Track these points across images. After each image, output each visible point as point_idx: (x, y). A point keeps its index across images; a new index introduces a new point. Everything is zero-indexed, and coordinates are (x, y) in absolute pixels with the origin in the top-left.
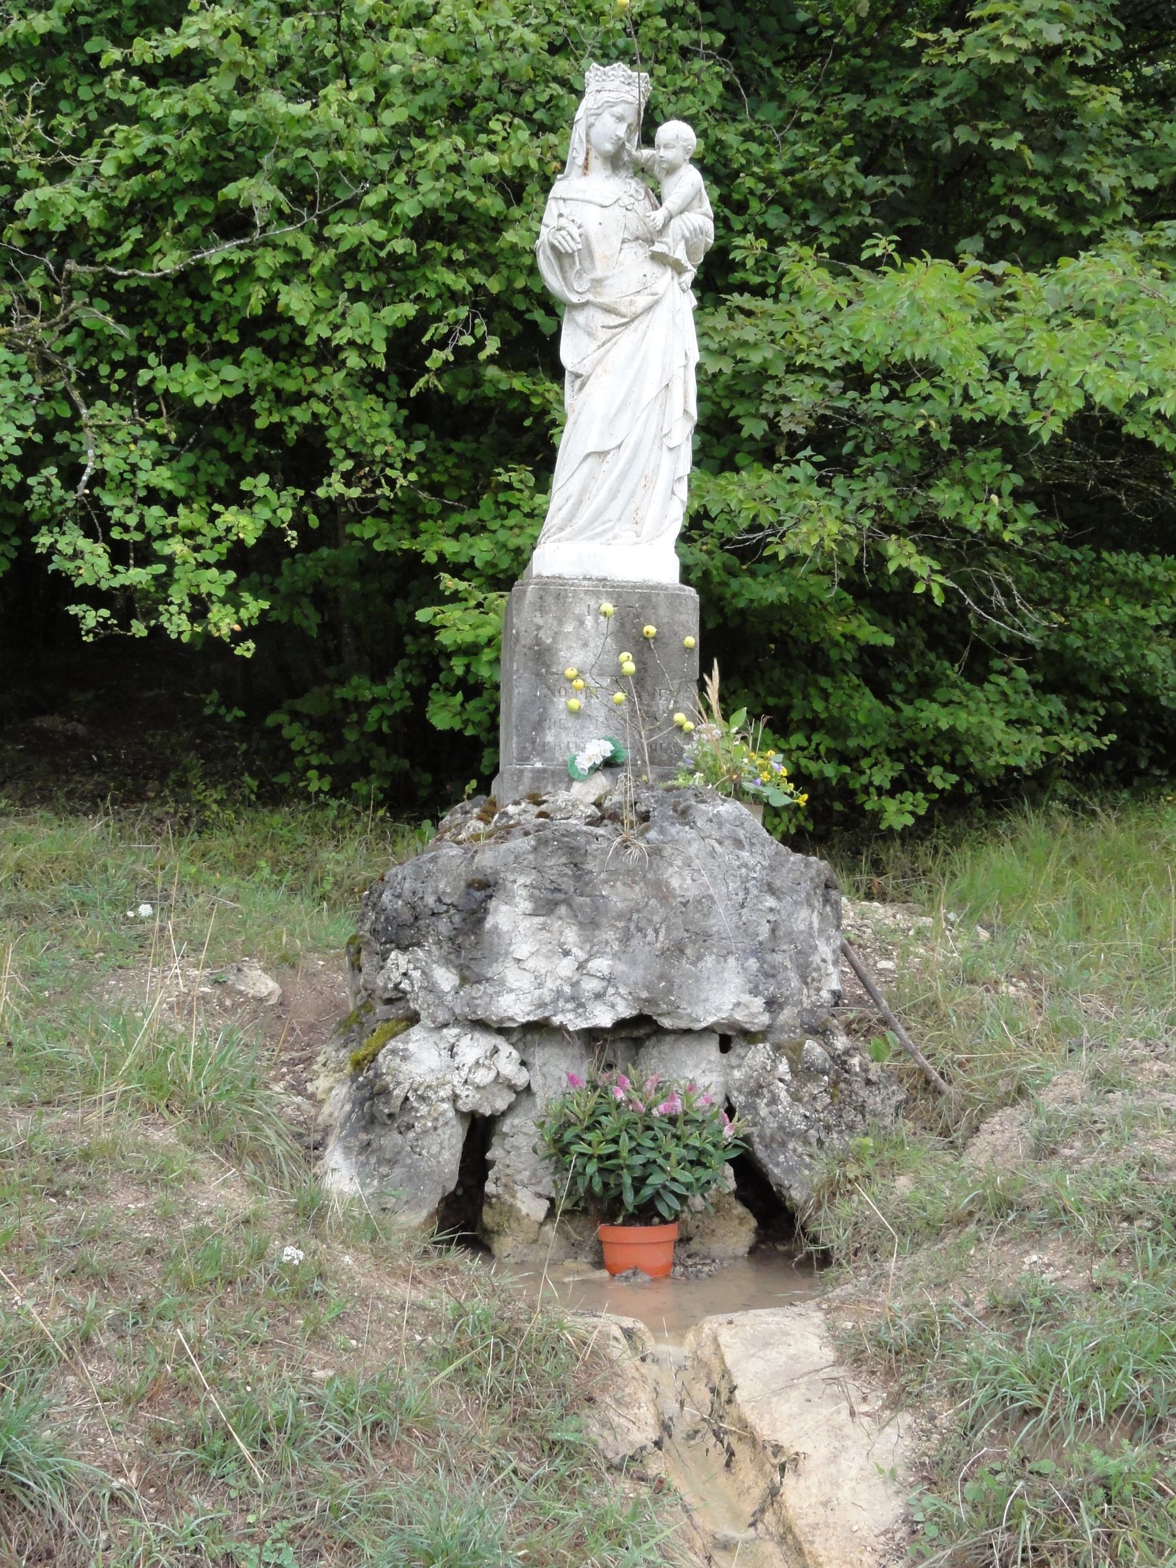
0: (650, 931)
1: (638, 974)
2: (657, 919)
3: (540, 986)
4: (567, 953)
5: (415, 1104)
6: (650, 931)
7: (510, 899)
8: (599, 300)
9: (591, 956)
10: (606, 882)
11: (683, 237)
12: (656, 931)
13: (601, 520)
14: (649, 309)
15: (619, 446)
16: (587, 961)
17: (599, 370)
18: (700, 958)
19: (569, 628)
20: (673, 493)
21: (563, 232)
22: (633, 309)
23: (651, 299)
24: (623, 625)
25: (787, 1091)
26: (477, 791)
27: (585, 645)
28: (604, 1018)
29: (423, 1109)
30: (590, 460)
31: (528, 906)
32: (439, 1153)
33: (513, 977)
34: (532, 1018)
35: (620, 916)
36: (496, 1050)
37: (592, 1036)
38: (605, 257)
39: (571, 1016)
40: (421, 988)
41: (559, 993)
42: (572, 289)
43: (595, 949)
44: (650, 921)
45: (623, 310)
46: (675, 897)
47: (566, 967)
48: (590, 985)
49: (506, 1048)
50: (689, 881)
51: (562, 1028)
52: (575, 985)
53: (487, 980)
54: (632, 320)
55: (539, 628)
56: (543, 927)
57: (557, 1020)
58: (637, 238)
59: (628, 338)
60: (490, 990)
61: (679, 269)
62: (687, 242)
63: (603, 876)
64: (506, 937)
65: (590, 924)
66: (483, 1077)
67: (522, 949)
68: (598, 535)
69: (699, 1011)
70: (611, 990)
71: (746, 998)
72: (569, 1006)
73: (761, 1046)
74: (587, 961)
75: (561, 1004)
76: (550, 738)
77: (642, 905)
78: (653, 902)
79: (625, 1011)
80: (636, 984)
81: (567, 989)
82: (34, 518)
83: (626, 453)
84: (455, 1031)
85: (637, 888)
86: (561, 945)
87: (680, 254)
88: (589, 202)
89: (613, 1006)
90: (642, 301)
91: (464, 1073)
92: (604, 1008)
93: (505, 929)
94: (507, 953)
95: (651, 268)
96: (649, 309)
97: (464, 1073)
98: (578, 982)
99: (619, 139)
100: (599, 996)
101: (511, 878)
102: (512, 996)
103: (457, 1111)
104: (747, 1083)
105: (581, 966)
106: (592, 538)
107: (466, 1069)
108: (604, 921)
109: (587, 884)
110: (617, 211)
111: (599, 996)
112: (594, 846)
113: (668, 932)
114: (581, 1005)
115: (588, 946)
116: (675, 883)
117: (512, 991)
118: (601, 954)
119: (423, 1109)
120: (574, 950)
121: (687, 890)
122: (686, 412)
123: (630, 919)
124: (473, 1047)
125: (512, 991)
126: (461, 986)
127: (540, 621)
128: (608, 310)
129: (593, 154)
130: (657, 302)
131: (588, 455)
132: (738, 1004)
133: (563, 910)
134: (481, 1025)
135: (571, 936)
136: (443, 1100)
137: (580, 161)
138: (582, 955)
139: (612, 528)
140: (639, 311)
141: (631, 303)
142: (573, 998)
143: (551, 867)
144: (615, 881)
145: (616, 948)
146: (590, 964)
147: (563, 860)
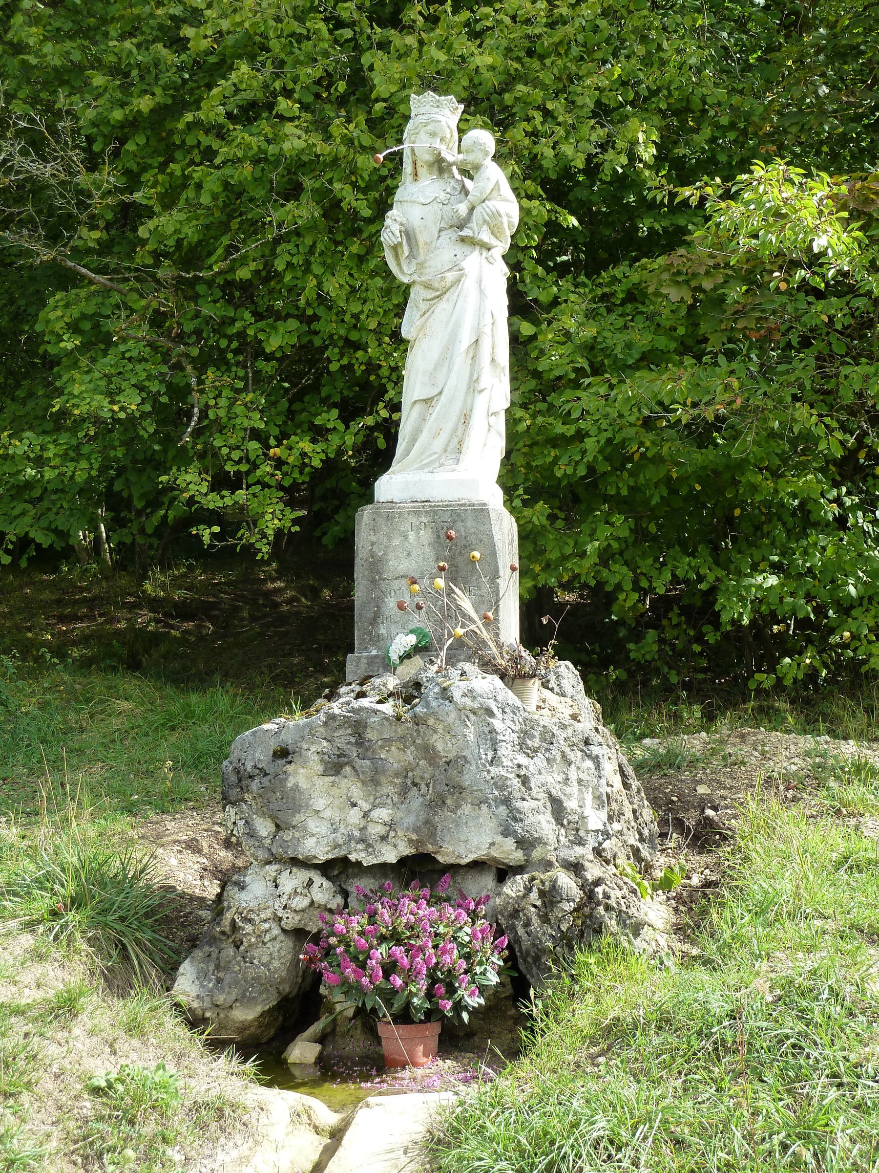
0: (423, 786)
1: (410, 820)
2: (427, 776)
3: (335, 831)
4: (354, 805)
5: (241, 924)
6: (423, 786)
7: (305, 764)
9: (374, 807)
10: (382, 747)
12: (428, 785)
15: (440, 393)
16: (370, 811)
18: (458, 807)
19: (396, 542)
22: (443, 284)
24: (438, 537)
25: (538, 915)
27: (409, 555)
28: (391, 856)
29: (249, 928)
31: (320, 768)
32: (270, 962)
33: (313, 825)
34: (330, 856)
35: (397, 775)
36: (310, 882)
37: (383, 869)
38: (426, 244)
39: (363, 854)
40: (244, 834)
41: (350, 838)
42: (403, 272)
43: (377, 801)
44: (422, 778)
45: (436, 285)
46: (441, 758)
47: (354, 816)
48: (376, 830)
49: (319, 880)
50: (450, 745)
51: (359, 864)
52: (363, 829)
53: (294, 827)
55: (373, 544)
56: (333, 784)
57: (353, 857)
58: (452, 227)
59: (443, 306)
60: (297, 835)
63: (380, 743)
64: (306, 792)
65: (373, 781)
66: (300, 903)
67: (320, 803)
69: (462, 850)
70: (392, 834)
71: (499, 839)
72: (360, 846)
73: (518, 877)
74: (370, 811)
75: (353, 844)
76: (382, 631)
77: (414, 765)
78: (422, 762)
79: (406, 850)
80: (408, 829)
81: (357, 833)
82: (273, 463)
84: (275, 867)
85: (408, 752)
86: (349, 799)
88: (414, 202)
89: (395, 846)
90: (450, 276)
91: (284, 900)
92: (389, 847)
93: (304, 786)
94: (307, 806)
95: (459, 249)
96: (458, 281)
97: (284, 900)
98: (365, 828)
100: (384, 838)
101: (305, 746)
102: (314, 839)
103: (284, 931)
104: (505, 908)
105: (366, 815)
106: (422, 468)
107: (286, 897)
108: (383, 779)
109: (367, 749)
110: (436, 206)
111: (384, 838)
112: (373, 720)
113: (434, 787)
114: (369, 845)
115: (372, 799)
116: (439, 746)
117: (313, 835)
118: (383, 805)
119: (249, 928)
120: (360, 802)
121: (449, 751)
123: (406, 777)
124: (290, 881)
125: (313, 835)
126: (277, 831)
127: (374, 539)
129: (419, 164)
131: (415, 402)
132: (493, 844)
133: (348, 770)
134: (296, 862)
135: (357, 792)
136: (265, 921)
138: (366, 806)
139: (439, 458)
141: (443, 278)
142: (362, 840)
143: (340, 737)
144: (390, 746)
145: (395, 799)
146: (372, 813)
147: (349, 731)
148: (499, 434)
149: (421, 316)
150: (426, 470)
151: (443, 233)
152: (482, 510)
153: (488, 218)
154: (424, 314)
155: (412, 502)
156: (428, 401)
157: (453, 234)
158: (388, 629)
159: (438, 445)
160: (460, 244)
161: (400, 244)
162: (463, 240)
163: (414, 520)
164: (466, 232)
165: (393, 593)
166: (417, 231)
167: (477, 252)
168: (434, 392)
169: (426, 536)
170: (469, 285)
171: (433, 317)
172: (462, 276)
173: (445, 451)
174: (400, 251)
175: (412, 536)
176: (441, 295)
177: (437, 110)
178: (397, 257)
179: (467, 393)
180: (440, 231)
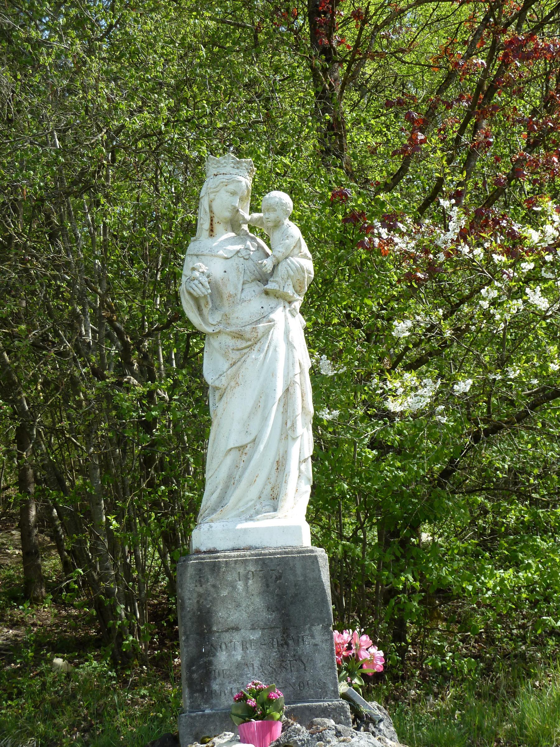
24: (268, 586)
30: (233, 453)
38: (230, 296)
45: (248, 336)
88: (216, 256)
95: (267, 302)
129: (215, 220)
131: (230, 450)
137: (207, 226)
148: (309, 480)
149: (232, 365)
151: (246, 286)
152: (310, 557)
153: (291, 273)
154: (234, 364)
155: (233, 550)
156: (241, 448)
157: (257, 288)
158: (222, 685)
159: (254, 492)
160: (264, 295)
162: (267, 293)
164: (271, 286)
165: (224, 647)
168: (250, 438)
169: (254, 585)
170: (277, 334)
172: (271, 327)
175: (240, 586)
176: (252, 345)
177: (237, 171)
179: (280, 439)
180: (243, 284)
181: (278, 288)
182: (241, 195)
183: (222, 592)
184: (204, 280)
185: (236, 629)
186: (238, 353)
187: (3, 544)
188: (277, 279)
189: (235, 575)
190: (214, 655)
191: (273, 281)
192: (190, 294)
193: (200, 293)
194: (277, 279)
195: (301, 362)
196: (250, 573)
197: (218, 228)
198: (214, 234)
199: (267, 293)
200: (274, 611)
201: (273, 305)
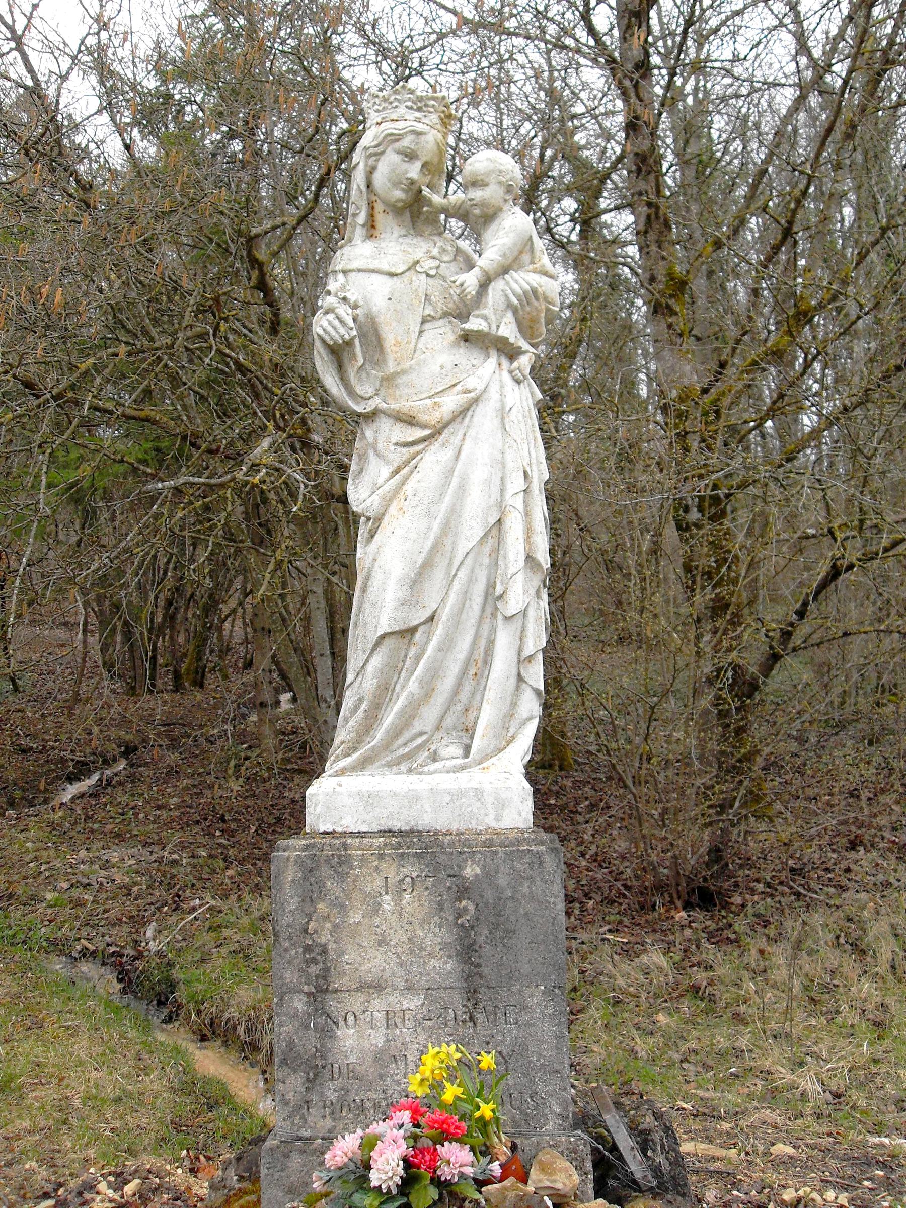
8: (394, 406)
11: (510, 305)
13: (407, 735)
14: (462, 413)
15: (432, 618)
17: (393, 510)
19: (355, 917)
20: (520, 678)
21: (331, 316)
23: (463, 399)
26: (816, 446)
30: (389, 643)
45: (423, 418)
54: (437, 432)
61: (511, 353)
62: (515, 312)
68: (408, 756)
83: (439, 631)
87: (508, 330)
90: (450, 403)
95: (465, 356)
96: (462, 413)
99: (412, 182)
122: (530, 559)
128: (410, 421)
129: (379, 207)
130: (476, 401)
131: (383, 637)
137: (362, 219)
140: (447, 417)
150: (403, 767)
151: (427, 326)
154: (397, 471)
160: (462, 343)
161: (349, 344)
162: (466, 338)
163: (391, 871)
166: (381, 319)
167: (493, 361)
171: (415, 476)
173: (438, 728)
174: (346, 357)
178: (340, 367)
180: (423, 322)
181: (486, 329)
182: (424, 159)
183: (351, 914)
184: (344, 311)
185: (377, 987)
186: (404, 450)
187: (2, 766)
188: (485, 312)
189: (379, 882)
190: (333, 1037)
191: (477, 316)
192: (323, 341)
193: (337, 337)
194: (485, 312)
195: (528, 470)
196: (408, 880)
197: (381, 219)
198: (376, 233)
199: (466, 338)
200: (450, 957)
201: (475, 362)
